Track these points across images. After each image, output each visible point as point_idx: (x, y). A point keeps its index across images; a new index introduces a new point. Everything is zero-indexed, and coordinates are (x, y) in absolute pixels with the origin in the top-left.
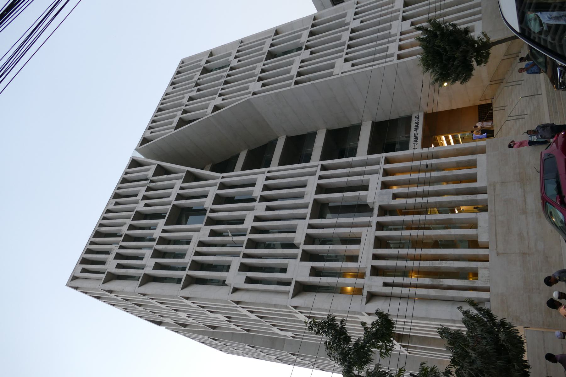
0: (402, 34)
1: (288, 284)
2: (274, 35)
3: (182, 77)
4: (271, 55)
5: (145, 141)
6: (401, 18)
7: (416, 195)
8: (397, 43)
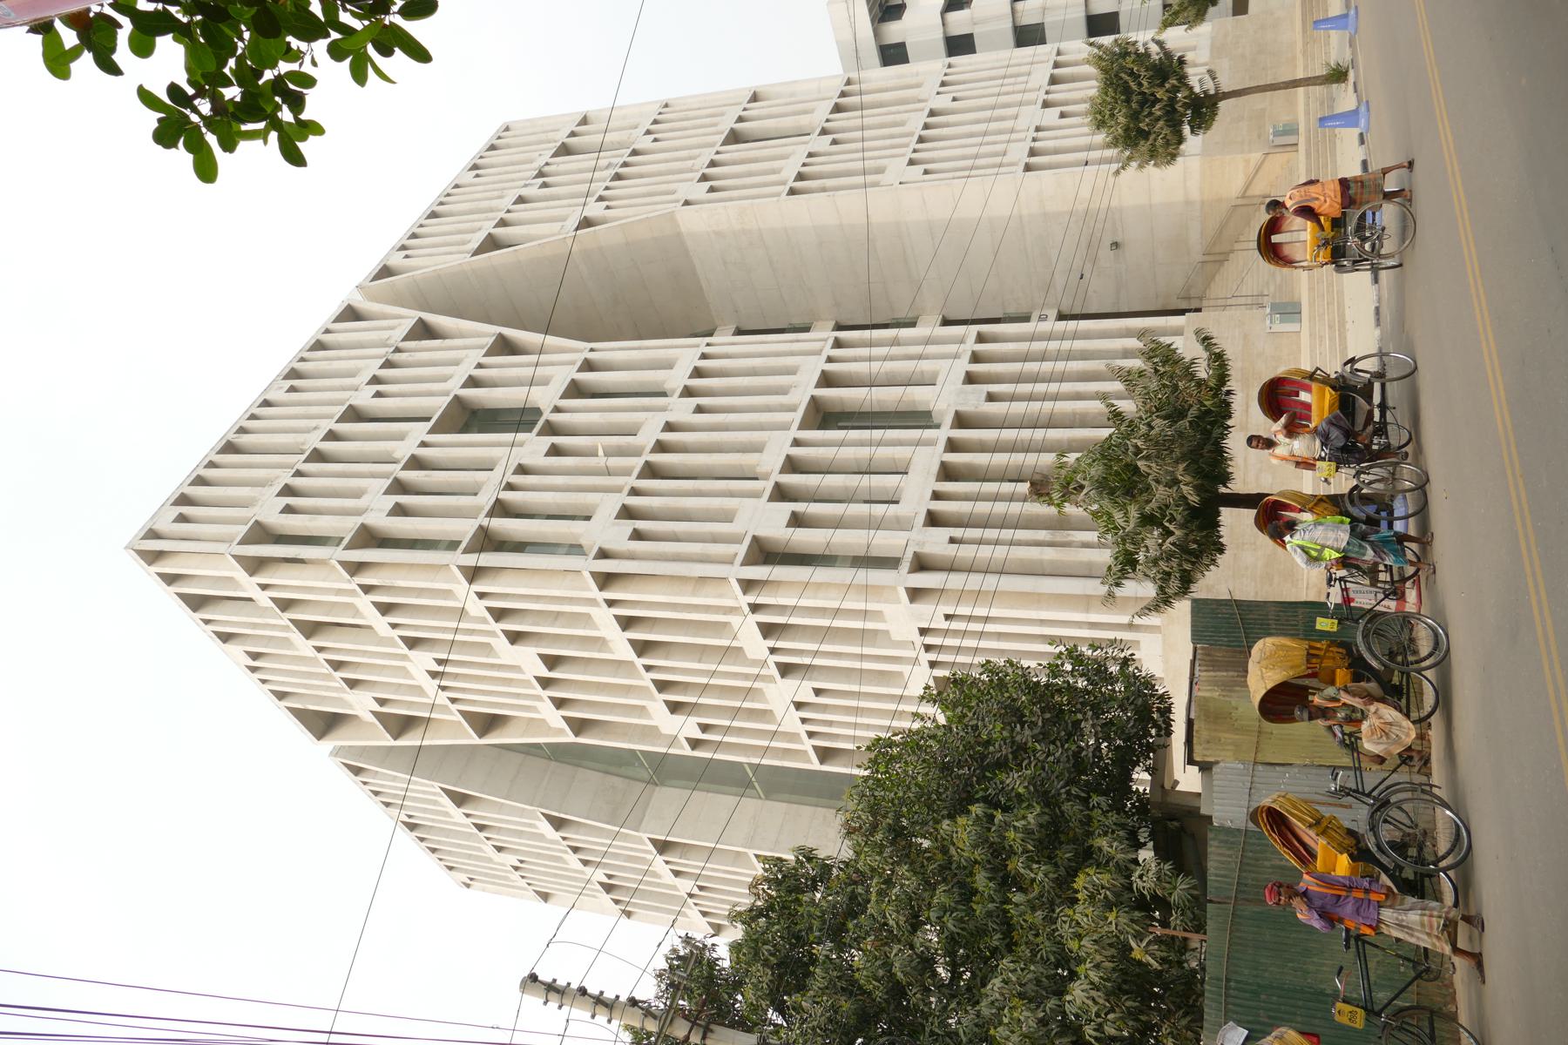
0: (1038, 129)
1: (737, 540)
2: (724, 144)
3: (494, 157)
4: (734, 138)
5: (385, 272)
6: (1040, 102)
7: (1013, 448)
8: (1029, 144)
